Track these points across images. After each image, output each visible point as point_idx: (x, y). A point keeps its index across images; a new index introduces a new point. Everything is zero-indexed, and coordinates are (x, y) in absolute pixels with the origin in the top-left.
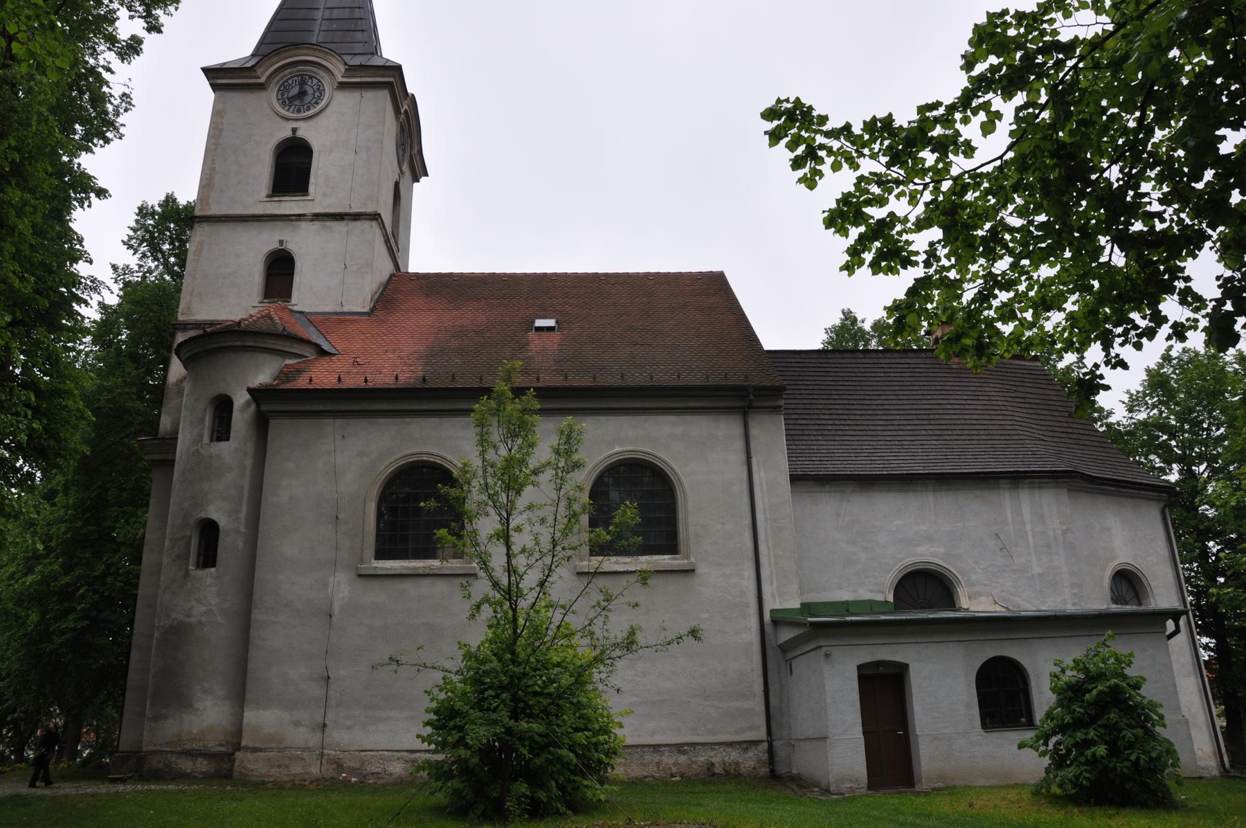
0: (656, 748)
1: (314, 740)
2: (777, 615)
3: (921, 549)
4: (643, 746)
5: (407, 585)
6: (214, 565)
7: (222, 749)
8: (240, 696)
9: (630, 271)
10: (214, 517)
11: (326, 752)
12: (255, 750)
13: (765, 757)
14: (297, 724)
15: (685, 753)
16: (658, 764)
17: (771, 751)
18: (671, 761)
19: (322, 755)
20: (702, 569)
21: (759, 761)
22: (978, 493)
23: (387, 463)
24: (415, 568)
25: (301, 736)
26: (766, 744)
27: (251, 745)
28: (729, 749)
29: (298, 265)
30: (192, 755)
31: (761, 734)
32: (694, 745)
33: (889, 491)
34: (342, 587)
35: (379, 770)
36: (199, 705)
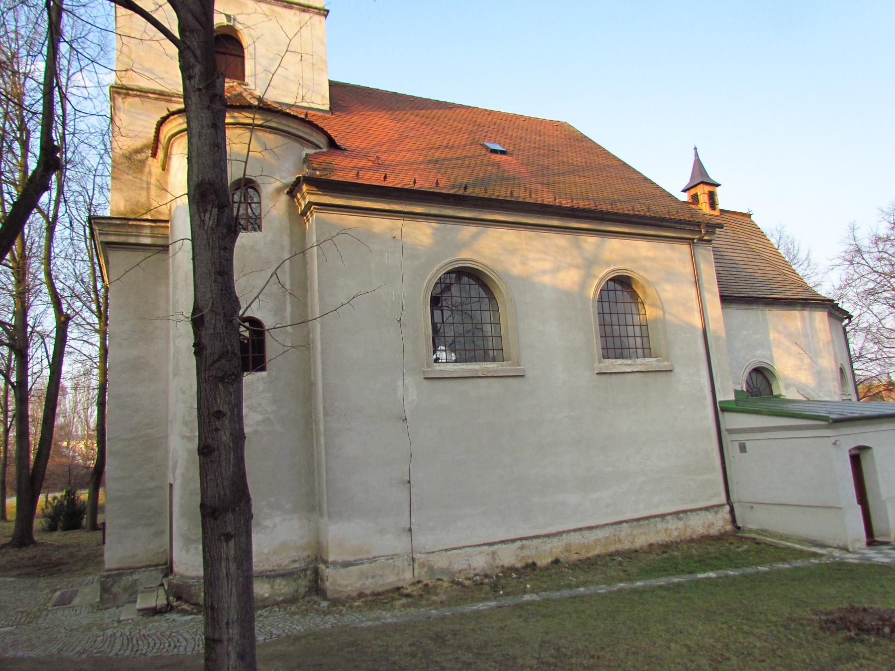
0: (663, 516)
1: (401, 545)
2: (723, 405)
3: (758, 352)
4: (655, 516)
5: (467, 385)
6: (263, 369)
7: (296, 565)
8: (312, 503)
9: (399, 92)
10: (258, 315)
11: (417, 556)
12: (346, 565)
13: (728, 516)
14: (383, 531)
15: (680, 519)
16: (666, 530)
17: (732, 511)
18: (674, 527)
19: (413, 560)
20: (677, 369)
21: (725, 520)
22: (744, 309)
23: (437, 267)
24: (470, 370)
25: (391, 543)
26: (727, 508)
27: (340, 559)
28: (707, 513)
29: (246, 41)
30: (268, 577)
31: (722, 499)
32: (684, 512)
33: (738, 309)
34: (411, 391)
35: (465, 566)
36: (268, 523)
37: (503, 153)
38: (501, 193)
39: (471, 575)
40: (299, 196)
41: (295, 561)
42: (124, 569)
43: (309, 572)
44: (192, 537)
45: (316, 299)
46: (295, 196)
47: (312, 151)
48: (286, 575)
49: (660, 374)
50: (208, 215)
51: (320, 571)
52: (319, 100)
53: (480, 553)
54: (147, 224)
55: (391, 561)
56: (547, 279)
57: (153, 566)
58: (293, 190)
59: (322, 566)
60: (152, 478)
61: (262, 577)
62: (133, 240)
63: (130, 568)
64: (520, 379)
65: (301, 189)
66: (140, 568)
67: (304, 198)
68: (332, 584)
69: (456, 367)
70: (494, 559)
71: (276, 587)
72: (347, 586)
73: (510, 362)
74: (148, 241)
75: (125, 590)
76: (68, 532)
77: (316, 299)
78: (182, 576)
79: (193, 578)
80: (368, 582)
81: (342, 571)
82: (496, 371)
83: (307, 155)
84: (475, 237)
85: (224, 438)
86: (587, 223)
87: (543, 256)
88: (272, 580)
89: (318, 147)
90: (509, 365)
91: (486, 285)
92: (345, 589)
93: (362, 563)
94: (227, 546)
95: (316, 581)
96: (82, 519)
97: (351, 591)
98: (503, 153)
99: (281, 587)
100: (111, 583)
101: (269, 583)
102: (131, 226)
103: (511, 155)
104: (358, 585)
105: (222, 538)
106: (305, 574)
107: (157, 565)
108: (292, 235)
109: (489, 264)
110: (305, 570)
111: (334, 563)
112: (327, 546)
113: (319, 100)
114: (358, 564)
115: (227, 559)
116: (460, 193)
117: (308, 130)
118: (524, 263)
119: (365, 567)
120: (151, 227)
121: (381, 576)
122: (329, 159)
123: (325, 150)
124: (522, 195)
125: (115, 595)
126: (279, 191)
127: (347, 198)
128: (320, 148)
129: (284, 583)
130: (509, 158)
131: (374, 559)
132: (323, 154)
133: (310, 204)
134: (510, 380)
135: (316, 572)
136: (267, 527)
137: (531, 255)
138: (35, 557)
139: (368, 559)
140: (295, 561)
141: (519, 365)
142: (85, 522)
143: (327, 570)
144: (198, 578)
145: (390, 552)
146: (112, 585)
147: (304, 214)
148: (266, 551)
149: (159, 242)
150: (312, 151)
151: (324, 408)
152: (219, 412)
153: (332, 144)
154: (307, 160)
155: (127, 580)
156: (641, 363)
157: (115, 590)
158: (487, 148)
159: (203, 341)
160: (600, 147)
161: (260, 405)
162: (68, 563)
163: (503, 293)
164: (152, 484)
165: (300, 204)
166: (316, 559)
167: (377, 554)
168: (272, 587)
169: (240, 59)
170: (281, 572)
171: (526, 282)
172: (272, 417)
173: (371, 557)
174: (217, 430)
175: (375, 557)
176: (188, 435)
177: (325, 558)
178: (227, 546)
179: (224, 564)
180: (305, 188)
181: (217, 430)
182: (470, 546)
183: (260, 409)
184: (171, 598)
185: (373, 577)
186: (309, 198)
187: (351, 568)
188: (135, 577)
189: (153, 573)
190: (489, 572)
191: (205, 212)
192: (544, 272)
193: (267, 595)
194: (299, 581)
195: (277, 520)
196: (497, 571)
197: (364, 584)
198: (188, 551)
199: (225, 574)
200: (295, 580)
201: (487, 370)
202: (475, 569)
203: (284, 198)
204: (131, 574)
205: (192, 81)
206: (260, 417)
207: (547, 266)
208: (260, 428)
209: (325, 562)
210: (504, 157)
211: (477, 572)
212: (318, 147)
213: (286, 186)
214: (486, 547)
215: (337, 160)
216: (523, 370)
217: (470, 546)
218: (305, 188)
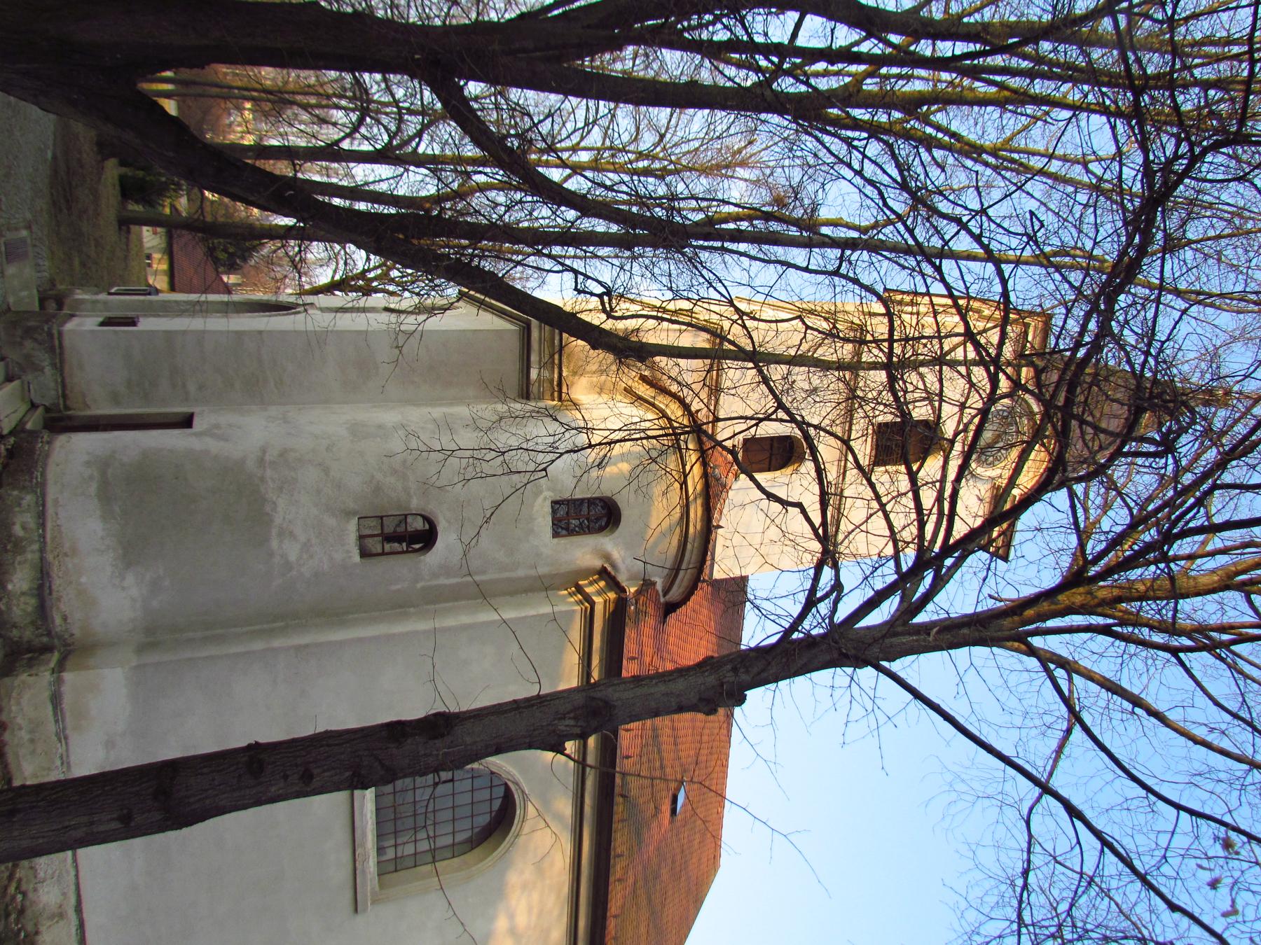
7: (58, 620)
12: (56, 700)
27: (66, 689)
30: (41, 587)
35: (42, 875)
36: (130, 579)
37: (674, 811)
38: (620, 842)
39: (24, 887)
40: (602, 584)
41: (65, 618)
42: (61, 354)
43: (45, 639)
44: (110, 471)
45: (465, 619)
46: (601, 579)
47: (659, 587)
48: (43, 611)
49: (349, 830)
50: (572, 722)
51: (48, 655)
52: (723, 566)
53: (64, 894)
54: (556, 376)
55: (58, 763)
56: (502, 924)
57: (64, 391)
58: (606, 575)
59: (56, 656)
60: (201, 387)
61: (42, 578)
62: (534, 358)
63: (62, 361)
64: (351, 908)
65: (611, 590)
66: (62, 375)
67: (599, 593)
68: (23, 682)
69: (369, 815)
70: (52, 917)
71: (22, 599)
72: (19, 704)
73: (377, 888)
74: (534, 374)
75: (28, 357)
76: (118, 188)
77: (465, 619)
78: (47, 456)
79: (43, 474)
80: (24, 735)
81: (46, 694)
82: (363, 871)
83: (654, 584)
84: (558, 817)
85: (273, 789)
86: (586, 927)
87: (535, 911)
88: (35, 592)
89: (665, 593)
90: (373, 889)
91: (490, 835)
92: (12, 702)
93: (57, 721)
94: (112, 819)
95: (29, 650)
96: (137, 202)
97: (10, 711)
98: (674, 811)
99: (22, 606)
100: (39, 338)
101: (30, 589)
102: (552, 356)
103: (671, 822)
104: (19, 720)
105: (125, 811)
106: (42, 635)
107: (65, 396)
108: (552, 576)
109: (521, 840)
110: (49, 634)
111: (59, 682)
112: (87, 668)
113: (723, 566)
114: (55, 714)
115: (92, 823)
116: (617, 790)
117: (685, 583)
118: (524, 887)
119: (52, 727)
120: (552, 380)
121: (33, 752)
122: (651, 610)
123: (662, 600)
124: (617, 869)
125: (21, 344)
126: (607, 557)
127: (602, 649)
128: (664, 596)
129: (30, 609)
130: (666, 822)
131: (62, 736)
132: (657, 599)
133: (592, 604)
134: (349, 894)
135: (48, 649)
136: (124, 579)
137: (535, 896)
138: (82, 167)
139: (64, 728)
140: (65, 618)
141: (373, 902)
142: (135, 208)
143: (47, 674)
144: (65, 762)
145: (72, 758)
146: (36, 340)
147: (580, 589)
148: (83, 580)
149: (534, 389)
150: (659, 587)
151: (307, 646)
152: (311, 777)
153: (670, 608)
154: (647, 584)
155: (45, 360)
156: (371, 865)
157: (29, 344)
158: (678, 789)
159: (409, 741)
160: (690, 929)
161: (311, 557)
162: (69, 209)
163: (481, 866)
164: (192, 388)
165: (591, 584)
166: (67, 645)
167: (71, 741)
168: (23, 594)
169: (766, 466)
170: (48, 604)
171: (498, 892)
172: (294, 573)
173: (68, 732)
174: (286, 777)
175: (66, 738)
176: (267, 458)
177: (68, 664)
178: (112, 819)
179: (85, 819)
180: (612, 595)
181: (286, 777)
182: (77, 876)
183: (305, 556)
184: (12, 440)
185: (32, 741)
186: (598, 600)
187: (50, 708)
188: (48, 370)
189: (53, 392)
190: (29, 913)
191: (574, 718)
192: (511, 917)
193: (10, 587)
194: (31, 628)
195: (134, 592)
196: (30, 928)
197: (20, 729)
198: (88, 464)
199: (67, 823)
200: (33, 623)
201: (366, 860)
202: (35, 890)
203: (597, 563)
204: (53, 365)
205: (731, 674)
206: (293, 557)
207: (522, 920)
208: (277, 559)
209: (61, 667)
210: (668, 814)
211: (31, 895)
212: (665, 593)
213: (614, 566)
214: (73, 901)
215: (650, 622)
216: (365, 910)
217: (77, 876)
218: (612, 595)
